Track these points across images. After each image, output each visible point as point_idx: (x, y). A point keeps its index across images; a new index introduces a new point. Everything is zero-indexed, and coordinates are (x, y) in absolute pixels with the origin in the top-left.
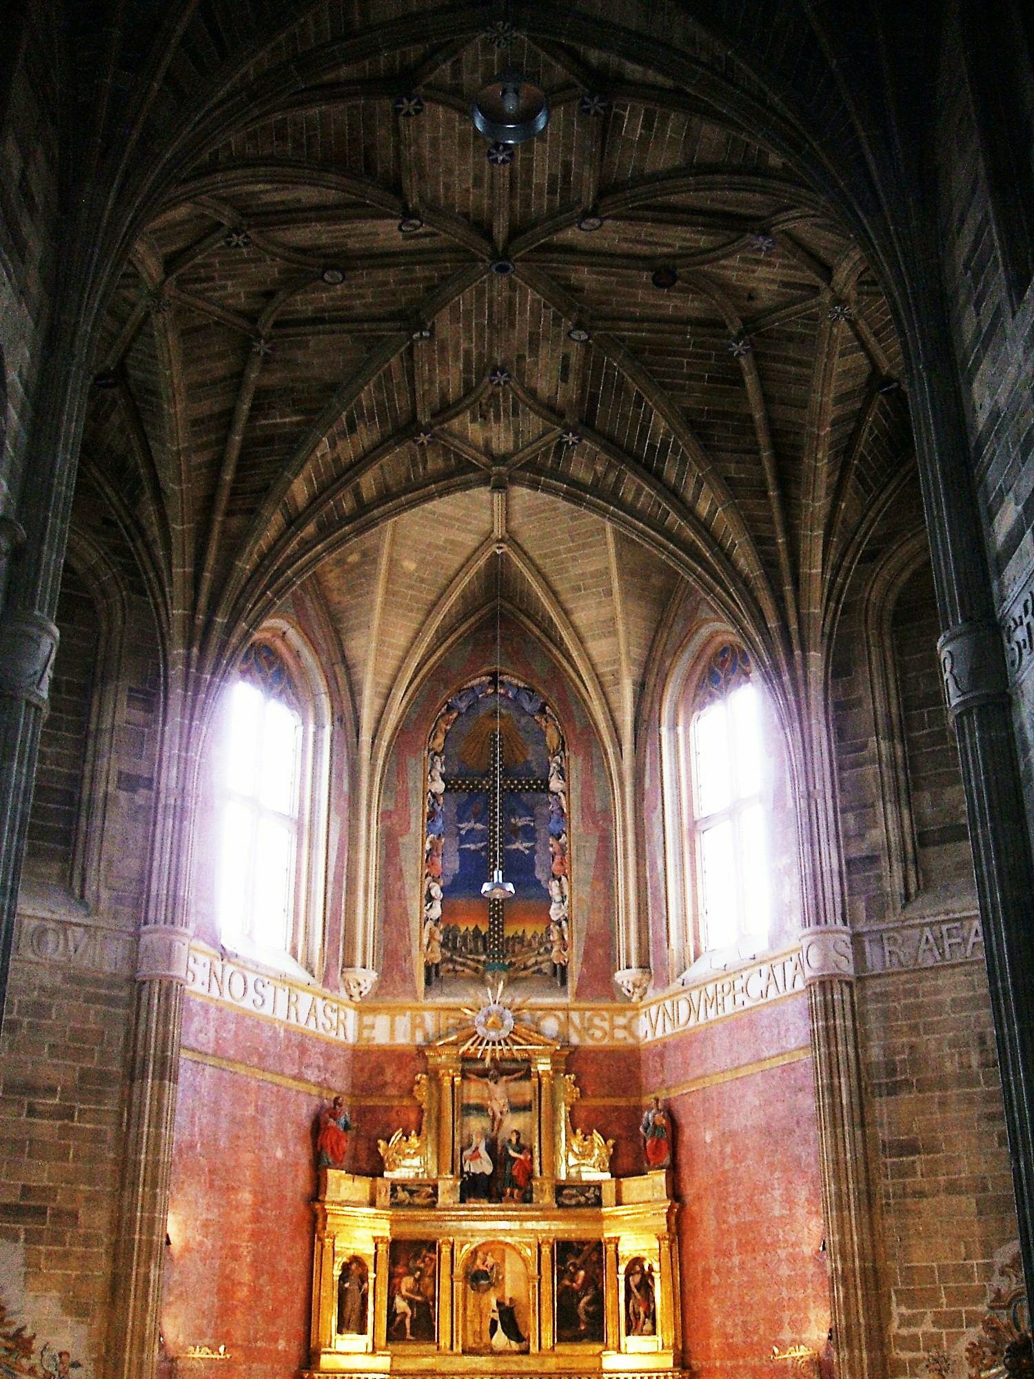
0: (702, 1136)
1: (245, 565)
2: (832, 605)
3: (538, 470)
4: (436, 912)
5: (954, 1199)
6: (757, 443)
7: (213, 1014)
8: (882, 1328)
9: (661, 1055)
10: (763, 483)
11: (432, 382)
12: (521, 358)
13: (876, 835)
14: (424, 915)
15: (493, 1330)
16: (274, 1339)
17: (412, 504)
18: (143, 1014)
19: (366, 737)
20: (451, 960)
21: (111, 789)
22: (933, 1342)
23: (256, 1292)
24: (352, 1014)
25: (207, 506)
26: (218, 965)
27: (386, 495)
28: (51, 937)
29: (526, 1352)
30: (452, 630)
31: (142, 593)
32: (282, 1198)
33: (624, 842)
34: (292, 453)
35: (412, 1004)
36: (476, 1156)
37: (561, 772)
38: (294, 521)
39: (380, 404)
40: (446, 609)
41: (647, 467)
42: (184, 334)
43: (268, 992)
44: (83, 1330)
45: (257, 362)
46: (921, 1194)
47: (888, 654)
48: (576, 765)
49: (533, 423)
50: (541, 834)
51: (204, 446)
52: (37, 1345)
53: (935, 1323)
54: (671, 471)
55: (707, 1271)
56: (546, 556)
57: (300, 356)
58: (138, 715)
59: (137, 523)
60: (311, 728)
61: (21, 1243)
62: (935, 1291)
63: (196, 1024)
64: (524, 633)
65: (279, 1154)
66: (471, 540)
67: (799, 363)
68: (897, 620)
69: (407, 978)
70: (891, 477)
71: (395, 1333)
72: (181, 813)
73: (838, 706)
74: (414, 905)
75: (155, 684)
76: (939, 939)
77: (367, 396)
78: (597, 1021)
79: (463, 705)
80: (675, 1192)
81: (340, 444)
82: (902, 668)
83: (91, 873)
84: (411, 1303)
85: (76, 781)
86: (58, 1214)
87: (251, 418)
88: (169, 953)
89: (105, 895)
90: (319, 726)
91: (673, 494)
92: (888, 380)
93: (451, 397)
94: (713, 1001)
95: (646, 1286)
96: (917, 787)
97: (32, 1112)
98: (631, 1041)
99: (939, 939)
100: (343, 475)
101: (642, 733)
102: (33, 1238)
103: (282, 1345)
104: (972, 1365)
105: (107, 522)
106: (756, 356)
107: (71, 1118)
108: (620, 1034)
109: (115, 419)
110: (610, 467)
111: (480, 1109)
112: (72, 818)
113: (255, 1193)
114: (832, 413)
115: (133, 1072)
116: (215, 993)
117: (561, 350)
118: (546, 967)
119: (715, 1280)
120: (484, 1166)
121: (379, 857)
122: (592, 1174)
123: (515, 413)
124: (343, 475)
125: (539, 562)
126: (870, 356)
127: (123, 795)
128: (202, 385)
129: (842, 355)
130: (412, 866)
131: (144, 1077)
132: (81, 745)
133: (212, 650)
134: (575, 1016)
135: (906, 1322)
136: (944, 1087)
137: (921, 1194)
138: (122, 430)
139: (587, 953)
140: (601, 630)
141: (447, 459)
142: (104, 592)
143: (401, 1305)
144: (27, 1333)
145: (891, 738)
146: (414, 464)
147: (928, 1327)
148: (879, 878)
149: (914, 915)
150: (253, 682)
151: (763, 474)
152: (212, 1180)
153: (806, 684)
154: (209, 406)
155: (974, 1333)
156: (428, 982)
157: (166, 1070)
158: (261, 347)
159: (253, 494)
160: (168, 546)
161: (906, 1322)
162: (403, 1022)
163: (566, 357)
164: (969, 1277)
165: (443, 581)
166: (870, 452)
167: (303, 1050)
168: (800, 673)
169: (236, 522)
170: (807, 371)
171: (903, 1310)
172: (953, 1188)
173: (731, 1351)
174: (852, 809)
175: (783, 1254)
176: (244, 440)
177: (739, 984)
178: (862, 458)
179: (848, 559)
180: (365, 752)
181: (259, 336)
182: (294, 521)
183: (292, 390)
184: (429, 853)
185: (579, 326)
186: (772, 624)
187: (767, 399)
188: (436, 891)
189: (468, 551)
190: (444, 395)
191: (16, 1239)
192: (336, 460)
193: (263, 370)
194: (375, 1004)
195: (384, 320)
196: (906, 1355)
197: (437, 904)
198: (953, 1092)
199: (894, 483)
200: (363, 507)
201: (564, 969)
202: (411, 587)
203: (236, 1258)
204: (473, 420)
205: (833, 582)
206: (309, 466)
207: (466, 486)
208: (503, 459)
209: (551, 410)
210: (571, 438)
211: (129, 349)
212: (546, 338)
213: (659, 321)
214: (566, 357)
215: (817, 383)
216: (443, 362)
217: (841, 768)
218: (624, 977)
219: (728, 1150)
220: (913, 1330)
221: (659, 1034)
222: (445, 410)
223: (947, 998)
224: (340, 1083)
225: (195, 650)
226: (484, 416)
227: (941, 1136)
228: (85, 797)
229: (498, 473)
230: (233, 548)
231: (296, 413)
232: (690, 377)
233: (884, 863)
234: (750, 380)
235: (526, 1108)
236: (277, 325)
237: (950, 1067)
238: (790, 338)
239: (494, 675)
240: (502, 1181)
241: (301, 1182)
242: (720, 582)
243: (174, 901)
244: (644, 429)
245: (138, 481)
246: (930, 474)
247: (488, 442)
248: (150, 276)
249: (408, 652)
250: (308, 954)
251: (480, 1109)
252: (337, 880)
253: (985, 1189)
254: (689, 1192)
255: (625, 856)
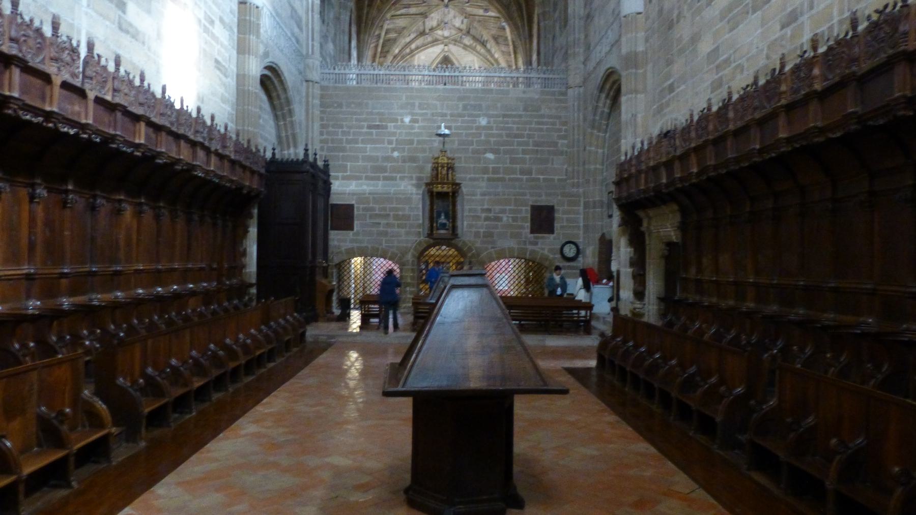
3: (456, 42)
49: (454, 32)
54: (488, 46)
91: (489, 51)
152: (340, 13)
169: (382, 59)
208: (446, 38)
209: (460, 30)
229: (445, 41)
246: (545, 120)
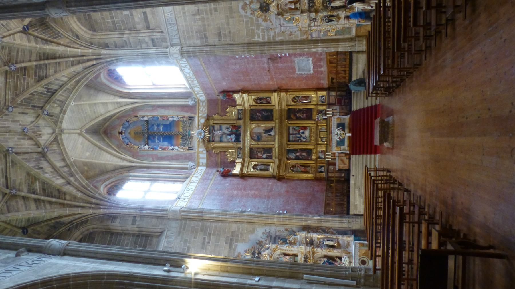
0: (225, 85)
1: (79, 195)
2: (90, 47)
3: (55, 120)
4: (176, 148)
5: (231, 24)
6: (44, 64)
7: (192, 200)
8: (261, 43)
9: (208, 94)
10: (56, 63)
11: (28, 148)
12: (20, 125)
13: (147, 39)
14: (177, 150)
15: (270, 135)
16: (268, 185)
17: (66, 153)
18: (189, 217)
19: (133, 164)
20: (188, 144)
21: (135, 226)
22: (263, 31)
23: (257, 190)
24: (199, 168)
25: (63, 205)
26: (181, 199)
27: (64, 160)
28: (169, 239)
29: (275, 127)
30: (108, 143)
31: (88, 220)
32: (238, 184)
33: (159, 102)
34: (48, 184)
35: (196, 154)
36: (231, 138)
37: (143, 117)
38: (69, 183)
39: (35, 161)
40: (102, 146)
41: (54, 93)
42: (9, 211)
43: (190, 187)
44: (258, 229)
45: (19, 193)
46: (230, 32)
47: (103, 33)
48: (141, 113)
50: (158, 122)
51: (45, 206)
52: (261, 239)
53: (259, 30)
55: (255, 84)
56: (86, 120)
57: (18, 182)
58: (118, 221)
59: (69, 223)
60: (130, 178)
61: (238, 244)
62: (251, 29)
63: (193, 204)
64: (108, 126)
65: (227, 184)
66: (81, 139)
67: (18, 52)
68: (95, 31)
69: (191, 154)
70: (56, 30)
71: (270, 157)
72: (142, 209)
73: (116, 47)
74: (174, 153)
75: (111, 216)
76: (170, 24)
77: (31, 165)
78: (201, 110)
79: (127, 141)
80: (237, 92)
81: (46, 171)
82: (106, 30)
83: (156, 230)
84: (264, 154)
85: (134, 235)
86: (232, 236)
87: (37, 194)
88: (175, 211)
89: (160, 227)
90: (131, 176)
92: (24, 28)
93: (34, 143)
94: (193, 82)
95: (260, 99)
96: (135, 28)
97: (209, 243)
98: (206, 101)
99: (170, 24)
100: (56, 170)
101: (132, 97)
102: (237, 241)
103: (270, 184)
104: (267, 21)
105: (69, 230)
106: (17, 63)
107: (211, 233)
108: (204, 104)
109: (39, 229)
110: (54, 102)
111: (221, 137)
112: (143, 235)
113: (235, 190)
114: (33, 44)
115: (202, 219)
116: (187, 200)
117: (17, 114)
118: (190, 121)
119: (257, 82)
120: (233, 136)
121: (163, 161)
122: (235, 112)
123: (39, 127)
124: (56, 170)
125: (87, 122)
126: (17, 33)
127: (137, 223)
128: (26, 207)
129: (15, 40)
130: (165, 154)
131: (202, 216)
132: (125, 234)
133: (102, 202)
134: (200, 115)
135: (259, 37)
136: (204, 25)
137: (230, 32)
138: (42, 227)
139: (185, 112)
140: (105, 106)
141: (54, 144)
142: (88, 230)
143: (264, 156)
144: (258, 242)
145: (123, 34)
146: (55, 153)
147: (260, 31)
148: (157, 39)
149: (165, 31)
150: (117, 192)
151: (53, 63)
153: (110, 54)
154: (33, 205)
155: (260, 20)
156: (192, 150)
157: (201, 211)
158: (14, 192)
159: (60, 194)
160: (74, 214)
161: (259, 37)
162: (201, 156)
163: (19, 113)
164: (248, 21)
165: (93, 146)
166: (48, 35)
167: (205, 179)
168: (107, 56)
169: (68, 197)
170: (20, 50)
171: (256, 37)
172: (228, 24)
173: (272, 79)
174: (141, 45)
175: (248, 66)
176: (43, 196)
177: (188, 75)
178: (49, 37)
179: (78, 42)
180: (137, 165)
181: (10, 193)
182: (69, 183)
183: (28, 184)
184: (162, 149)
185: (7, 109)
186: (94, 62)
187: (30, 61)
188: (171, 148)
189: (85, 140)
190: (33, 145)
191: (237, 245)
192: (51, 172)
193: (22, 191)
194: (197, 162)
195: (6, 160)
196: (266, 37)
197: (174, 147)
198: (206, 23)
199: (57, 29)
200: (67, 166)
201: (190, 117)
202: (94, 154)
203: (249, 194)
204: (41, 137)
205: (85, 47)
206: (52, 179)
207: (61, 139)
210: (46, 112)
211: (15, 226)
212: (13, 118)
213: (6, 88)
214: (19, 113)
215: (24, 48)
216: (21, 145)
217: (131, 47)
218: (190, 103)
219: (227, 78)
220: (260, 35)
221: (203, 95)
222: (38, 145)
223: (184, 24)
224: (214, 171)
225: (101, 207)
226: (40, 135)
227: (216, 26)
228: (137, 233)
230: (74, 198)
231: (36, 183)
232: (24, 81)
233: (153, 37)
234: (23, 65)
235: (221, 126)
236: (7, 188)
237: (200, 23)
238: (10, 54)
239: (120, 133)
240: (237, 133)
241: (235, 180)
242: (85, 76)
243: (162, 210)
244: (42, 93)
245: (57, 222)
247: (48, 134)
248: (280, 201)
249: (111, 154)
250: (184, 178)
251: (221, 137)
252: (167, 171)
253: (227, 16)
254: (239, 88)
255: (162, 102)
